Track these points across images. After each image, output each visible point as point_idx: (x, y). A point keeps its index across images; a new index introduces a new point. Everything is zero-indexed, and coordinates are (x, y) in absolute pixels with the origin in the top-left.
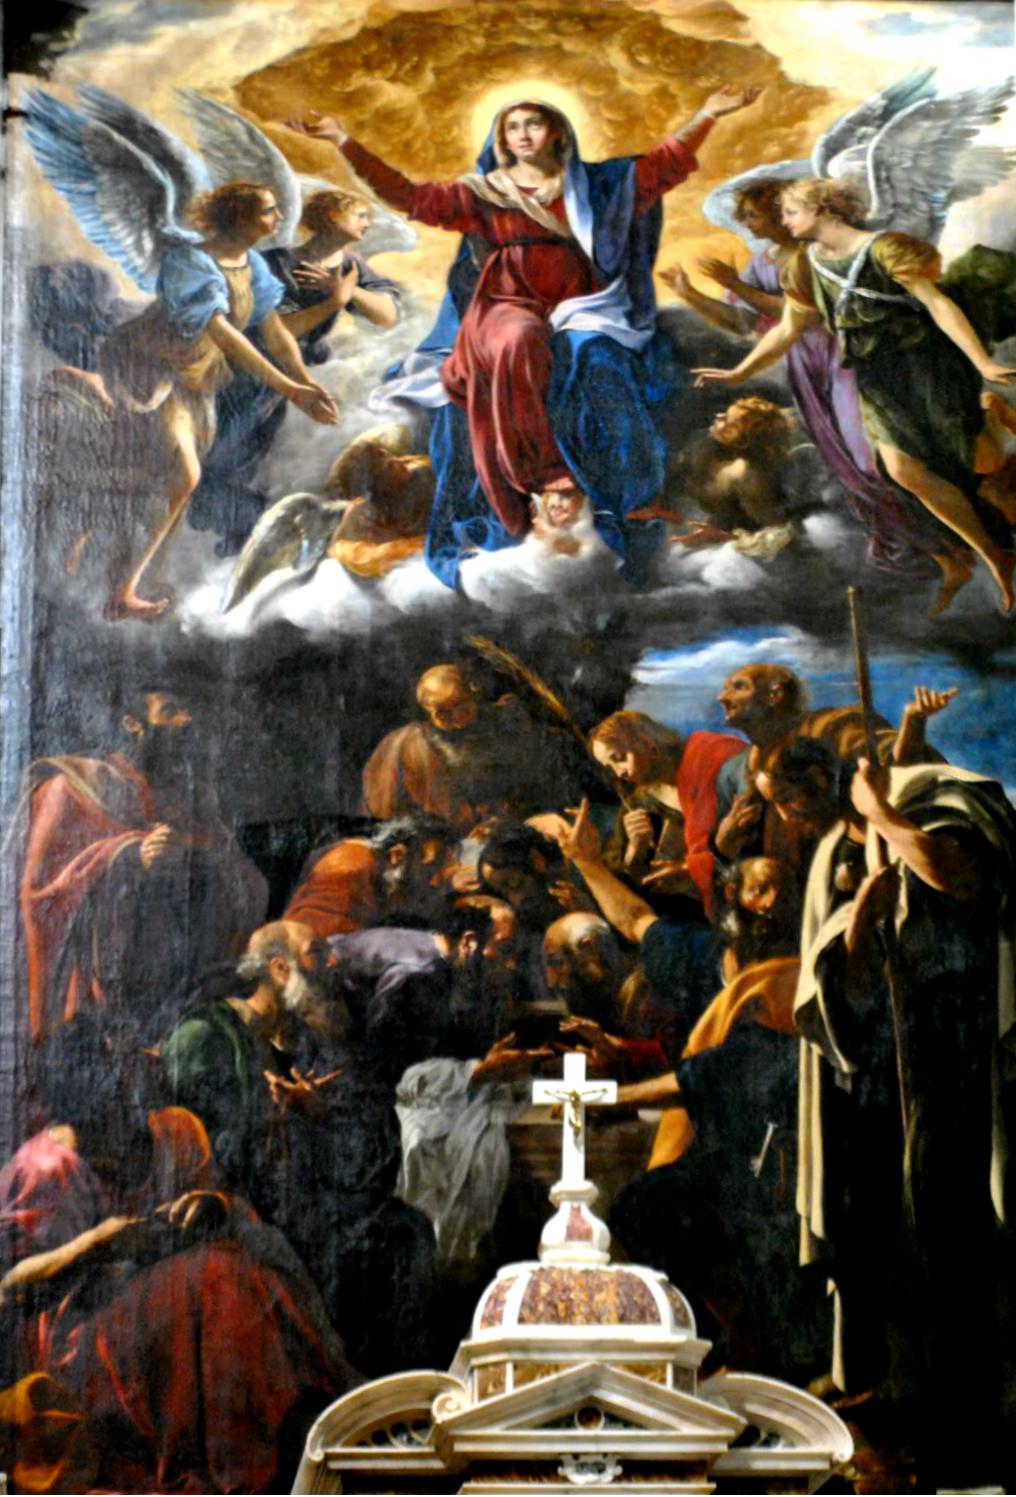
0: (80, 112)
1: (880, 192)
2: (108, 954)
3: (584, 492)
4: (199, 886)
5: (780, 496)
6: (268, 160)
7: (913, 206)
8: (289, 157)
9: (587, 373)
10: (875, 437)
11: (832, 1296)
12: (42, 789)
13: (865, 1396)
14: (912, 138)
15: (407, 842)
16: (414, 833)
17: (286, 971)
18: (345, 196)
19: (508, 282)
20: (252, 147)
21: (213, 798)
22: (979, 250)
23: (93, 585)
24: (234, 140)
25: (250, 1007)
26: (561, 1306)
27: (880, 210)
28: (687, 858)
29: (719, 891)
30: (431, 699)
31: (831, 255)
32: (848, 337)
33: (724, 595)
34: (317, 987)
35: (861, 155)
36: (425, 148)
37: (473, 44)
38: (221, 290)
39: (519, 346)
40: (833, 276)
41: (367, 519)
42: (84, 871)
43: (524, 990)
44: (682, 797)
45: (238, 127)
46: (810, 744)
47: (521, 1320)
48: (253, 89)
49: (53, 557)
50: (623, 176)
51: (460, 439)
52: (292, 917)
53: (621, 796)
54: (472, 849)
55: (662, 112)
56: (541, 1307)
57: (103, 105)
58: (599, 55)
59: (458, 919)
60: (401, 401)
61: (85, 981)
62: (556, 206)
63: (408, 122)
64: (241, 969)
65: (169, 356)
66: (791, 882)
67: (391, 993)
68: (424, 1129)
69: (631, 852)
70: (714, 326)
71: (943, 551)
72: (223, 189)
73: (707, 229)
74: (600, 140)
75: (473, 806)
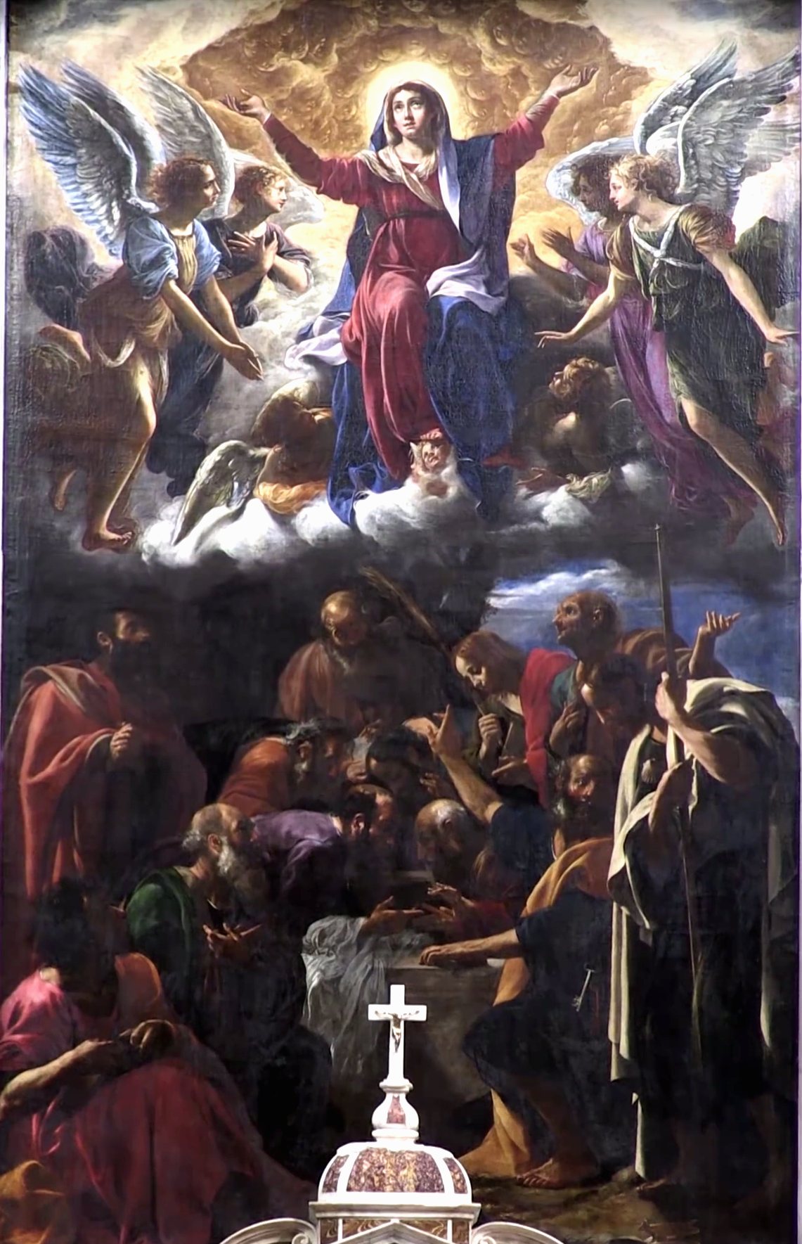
0: (64, 89)
1: (688, 169)
3: (451, 442)
6: (209, 136)
7: (713, 181)
9: (454, 334)
12: (36, 693)
13: (661, 1182)
14: (714, 116)
15: (312, 740)
16: (319, 732)
17: (219, 845)
18: (268, 171)
19: (393, 251)
24: (183, 117)
25: (195, 872)
27: (687, 185)
28: (528, 753)
29: (551, 780)
31: (647, 228)
32: (659, 302)
33: (558, 531)
34: (242, 858)
36: (330, 126)
38: (172, 257)
39: (401, 311)
40: (648, 247)
41: (283, 464)
43: (401, 863)
46: (623, 659)
48: (198, 67)
51: (355, 390)
53: (476, 703)
54: (362, 744)
58: (467, 37)
60: (310, 359)
62: (432, 181)
65: (131, 317)
66: (608, 777)
67: (300, 862)
70: (554, 293)
71: (729, 493)
74: (468, 118)
75: (362, 709)
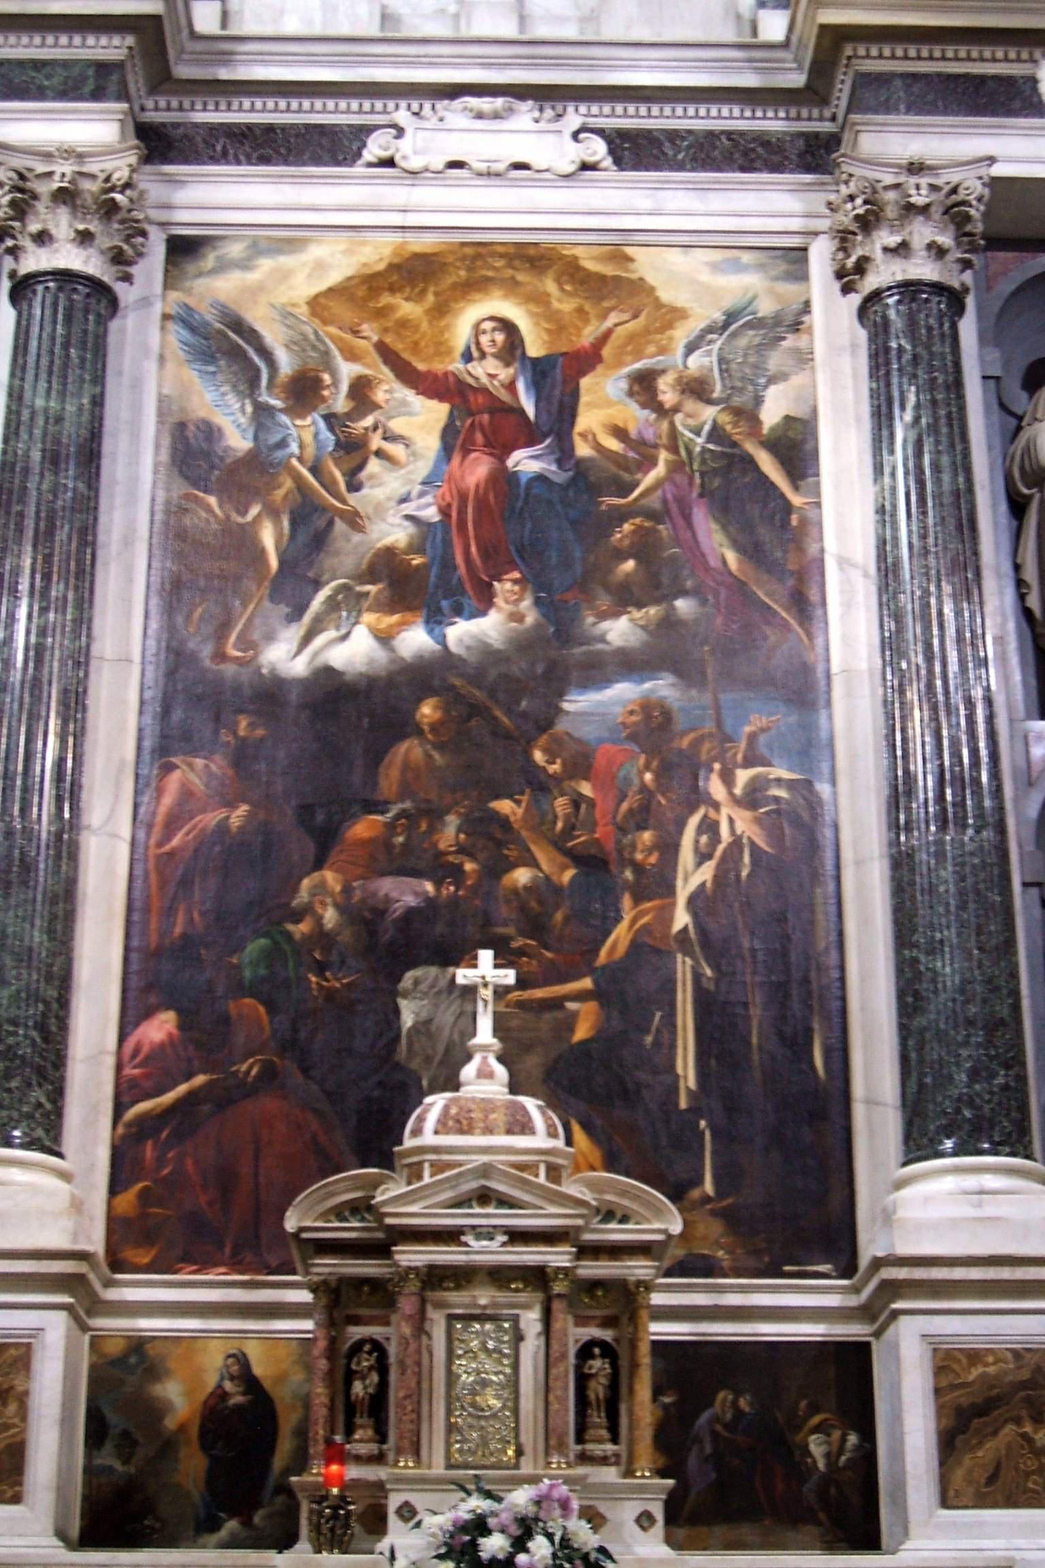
0: (209, 317)
1: (722, 379)
2: (203, 894)
4: (267, 847)
5: (658, 586)
6: (327, 353)
8: (341, 350)
10: (721, 545)
11: (703, 1133)
13: (730, 1201)
14: (743, 342)
19: (479, 438)
20: (317, 343)
21: (279, 787)
22: (788, 418)
23: (203, 641)
24: (305, 337)
25: (302, 929)
26: (465, 1122)
27: (722, 391)
29: (620, 852)
30: (426, 720)
35: (709, 353)
36: (426, 346)
37: (459, 276)
40: (691, 435)
42: (191, 836)
44: (594, 787)
45: (308, 330)
47: (436, 1132)
49: (180, 620)
50: (554, 367)
51: (447, 543)
52: (330, 869)
54: (452, 823)
55: (579, 323)
56: (451, 1123)
57: (222, 312)
58: (539, 284)
59: (442, 870)
60: (409, 518)
61: (189, 912)
62: (511, 387)
63: (416, 328)
64: (295, 903)
66: (669, 849)
67: (395, 921)
68: (417, 1014)
69: (560, 825)
70: (614, 469)
72: (298, 371)
73: (609, 403)
74: (540, 342)
